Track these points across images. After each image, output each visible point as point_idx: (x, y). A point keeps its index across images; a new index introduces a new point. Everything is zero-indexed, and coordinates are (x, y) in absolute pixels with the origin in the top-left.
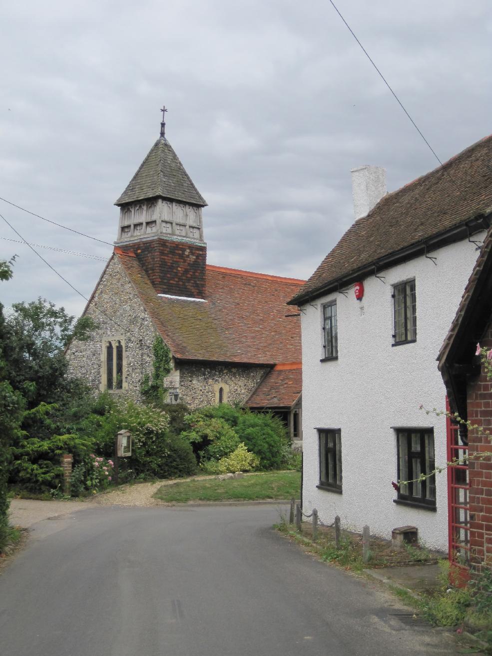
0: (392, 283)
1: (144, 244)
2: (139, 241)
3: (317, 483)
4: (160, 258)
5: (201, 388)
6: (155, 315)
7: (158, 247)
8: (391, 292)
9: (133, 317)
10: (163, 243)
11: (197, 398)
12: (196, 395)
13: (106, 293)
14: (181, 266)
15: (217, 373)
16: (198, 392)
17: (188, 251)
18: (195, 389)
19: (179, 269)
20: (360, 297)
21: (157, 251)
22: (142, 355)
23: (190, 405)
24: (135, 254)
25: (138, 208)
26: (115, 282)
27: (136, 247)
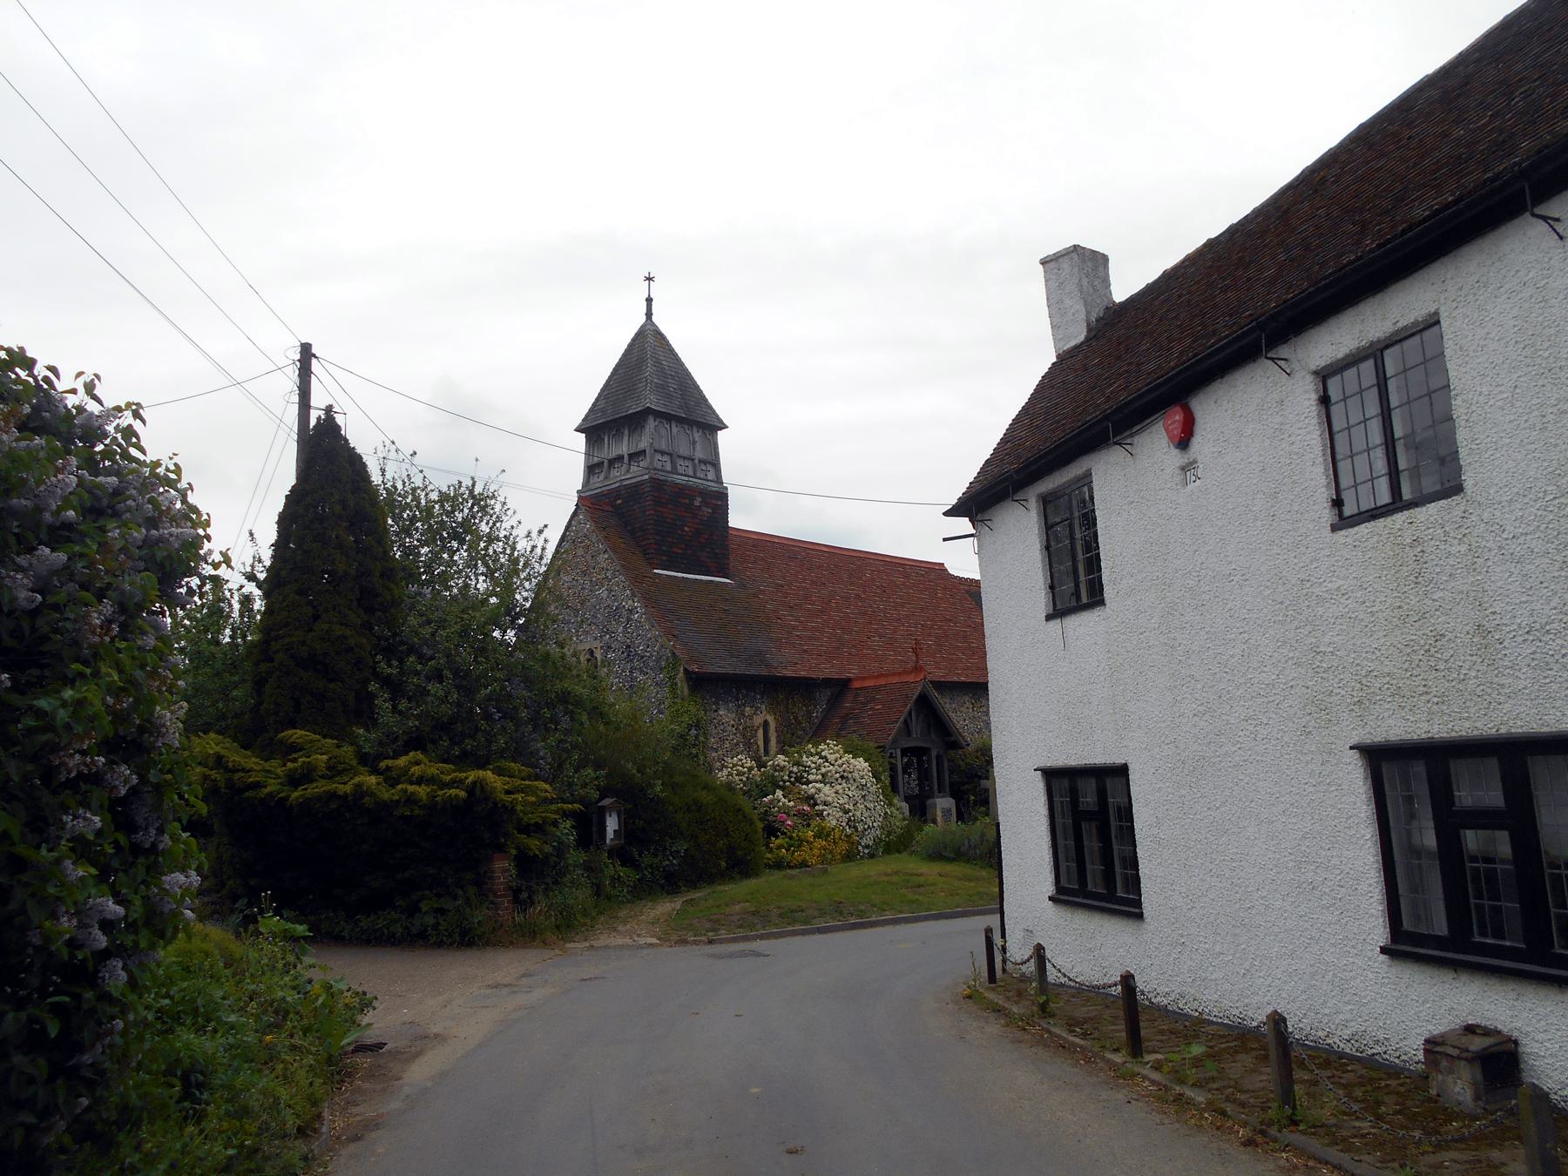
0: (1313, 368)
2: (617, 485)
3: (1049, 888)
4: (654, 510)
5: (732, 722)
6: (649, 601)
7: (651, 493)
8: (1317, 391)
10: (657, 485)
13: (567, 573)
14: (689, 524)
15: (758, 696)
17: (699, 499)
18: (723, 724)
19: (686, 529)
20: (1184, 440)
22: (631, 672)
23: (716, 752)
24: (612, 507)
25: (614, 433)
26: (580, 552)
27: (614, 494)
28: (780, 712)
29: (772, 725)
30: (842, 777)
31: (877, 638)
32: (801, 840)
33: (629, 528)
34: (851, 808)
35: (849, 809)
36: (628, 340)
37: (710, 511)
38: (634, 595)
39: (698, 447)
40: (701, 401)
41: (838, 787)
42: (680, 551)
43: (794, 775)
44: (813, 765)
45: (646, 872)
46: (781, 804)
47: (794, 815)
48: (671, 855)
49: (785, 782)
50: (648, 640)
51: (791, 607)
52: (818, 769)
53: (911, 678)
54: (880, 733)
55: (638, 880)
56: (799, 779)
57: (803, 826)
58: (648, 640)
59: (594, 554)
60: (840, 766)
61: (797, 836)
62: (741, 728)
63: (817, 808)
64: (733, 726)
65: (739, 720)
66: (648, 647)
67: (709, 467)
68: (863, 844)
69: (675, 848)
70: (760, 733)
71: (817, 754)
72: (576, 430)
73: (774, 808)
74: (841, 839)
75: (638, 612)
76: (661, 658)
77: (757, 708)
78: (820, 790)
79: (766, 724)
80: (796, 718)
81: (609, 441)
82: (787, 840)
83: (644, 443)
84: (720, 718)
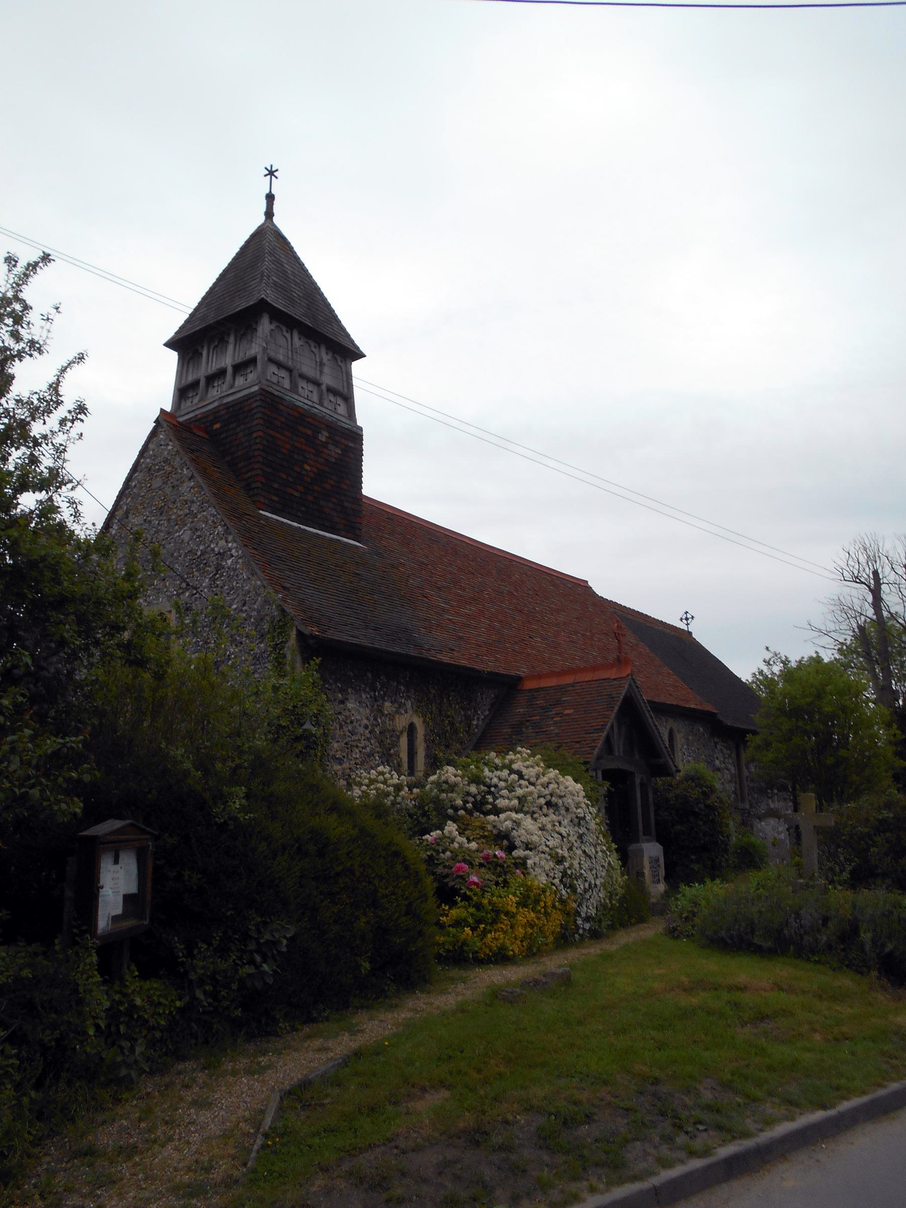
1: (228, 408)
2: (216, 404)
5: (365, 721)
9: (199, 553)
11: (357, 747)
12: (354, 738)
16: (361, 730)
17: (326, 434)
18: (352, 722)
21: (258, 415)
23: (340, 764)
25: (216, 343)
26: (157, 483)
28: (431, 713)
29: (421, 731)
30: (549, 804)
31: (539, 639)
32: (497, 911)
33: (228, 458)
34: (566, 854)
35: (563, 857)
36: (242, 243)
37: (339, 452)
38: (227, 531)
39: (326, 370)
40: (333, 321)
41: (544, 820)
42: (296, 494)
43: (471, 799)
44: (502, 784)
45: (199, 994)
46: (456, 845)
47: (481, 865)
48: (258, 951)
49: (456, 809)
50: (245, 595)
51: (438, 588)
52: (511, 789)
53: (612, 674)
54: (577, 746)
55: (181, 1010)
56: (480, 806)
57: (497, 884)
58: (245, 595)
59: (176, 483)
60: (546, 786)
61: (490, 903)
62: (377, 730)
63: (515, 853)
64: (366, 727)
65: (375, 719)
66: (244, 605)
67: (340, 401)
68: (583, 915)
69: (268, 936)
70: (404, 741)
71: (504, 767)
72: (167, 345)
73: (444, 852)
74: (554, 907)
75: (232, 556)
76: (262, 619)
77: (401, 705)
78: (517, 823)
79: (411, 728)
80: (452, 724)
81: (208, 356)
82: (472, 910)
83: (255, 348)
84: (348, 714)
